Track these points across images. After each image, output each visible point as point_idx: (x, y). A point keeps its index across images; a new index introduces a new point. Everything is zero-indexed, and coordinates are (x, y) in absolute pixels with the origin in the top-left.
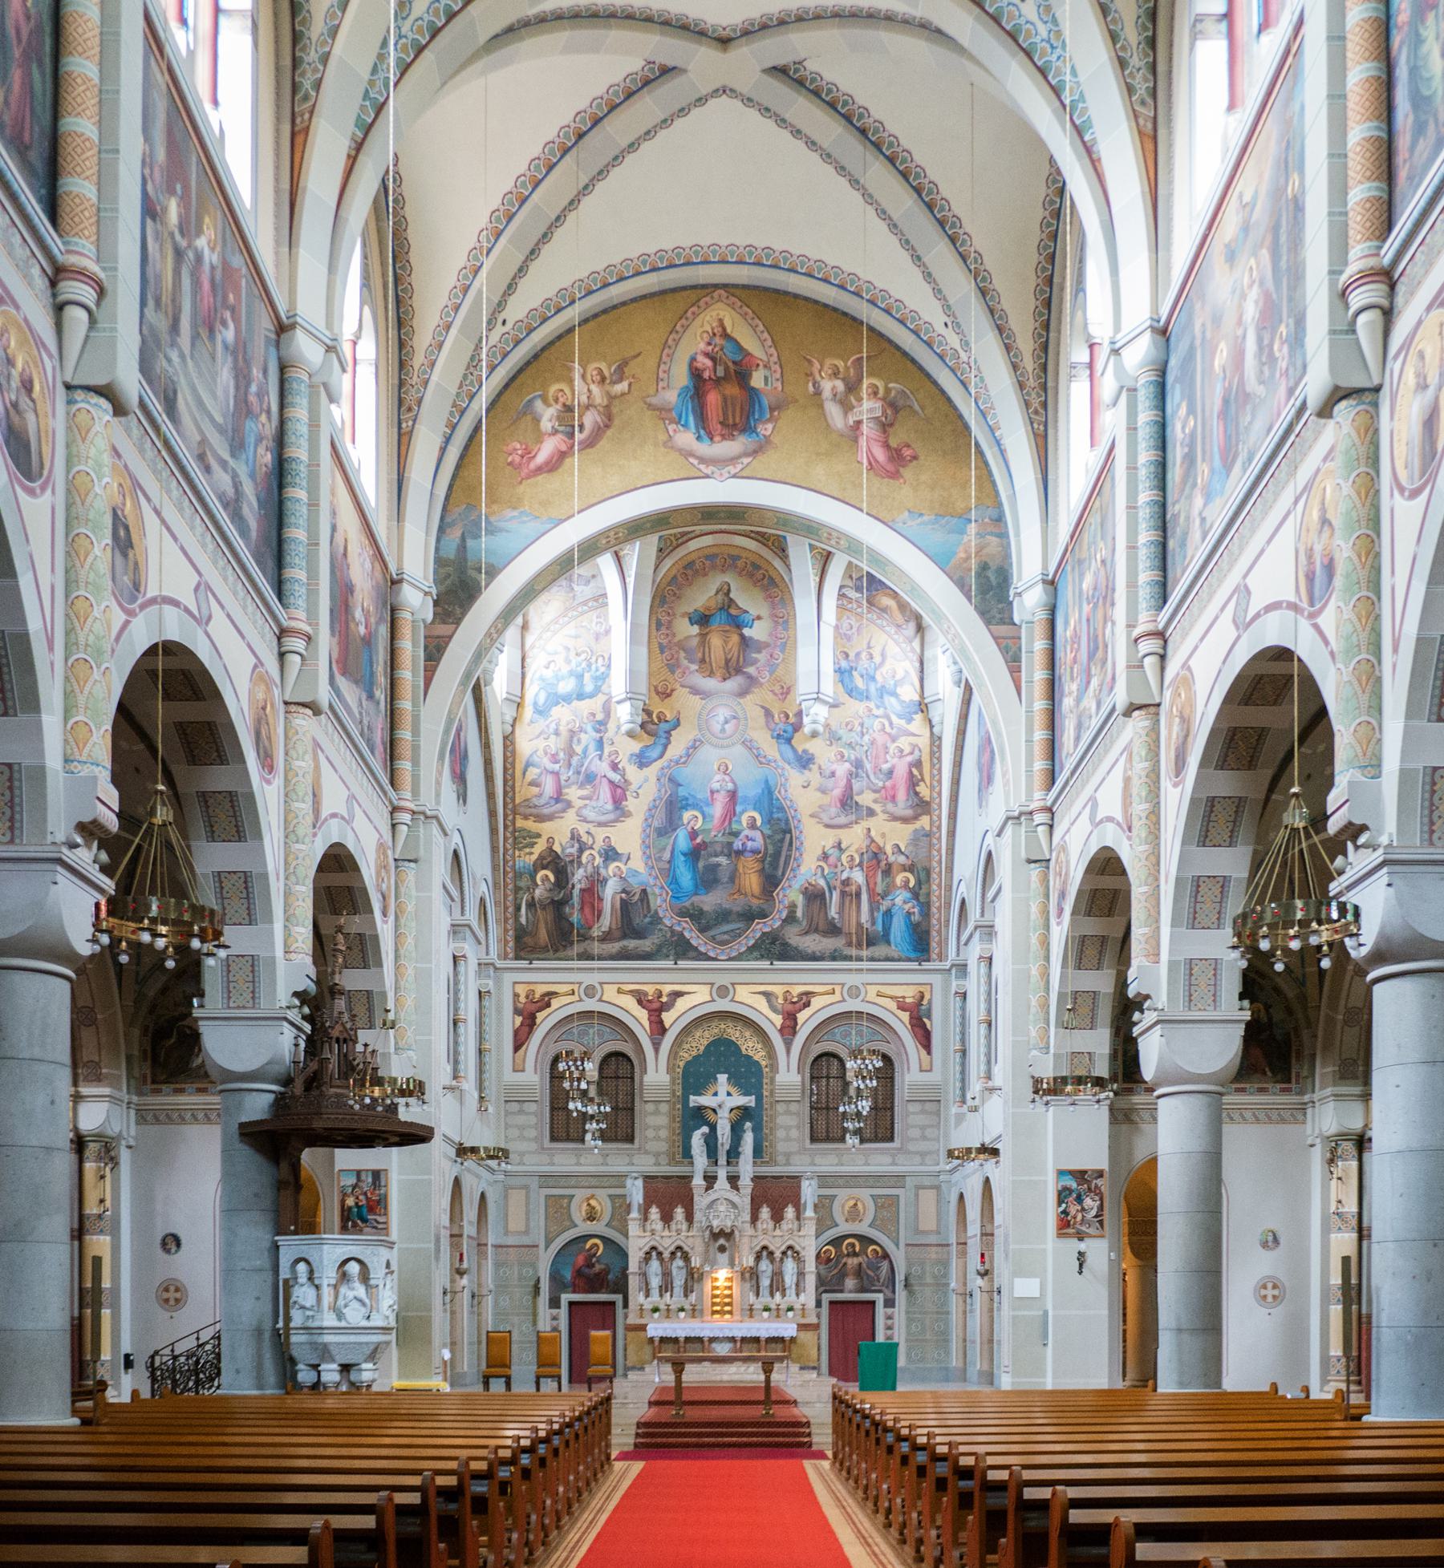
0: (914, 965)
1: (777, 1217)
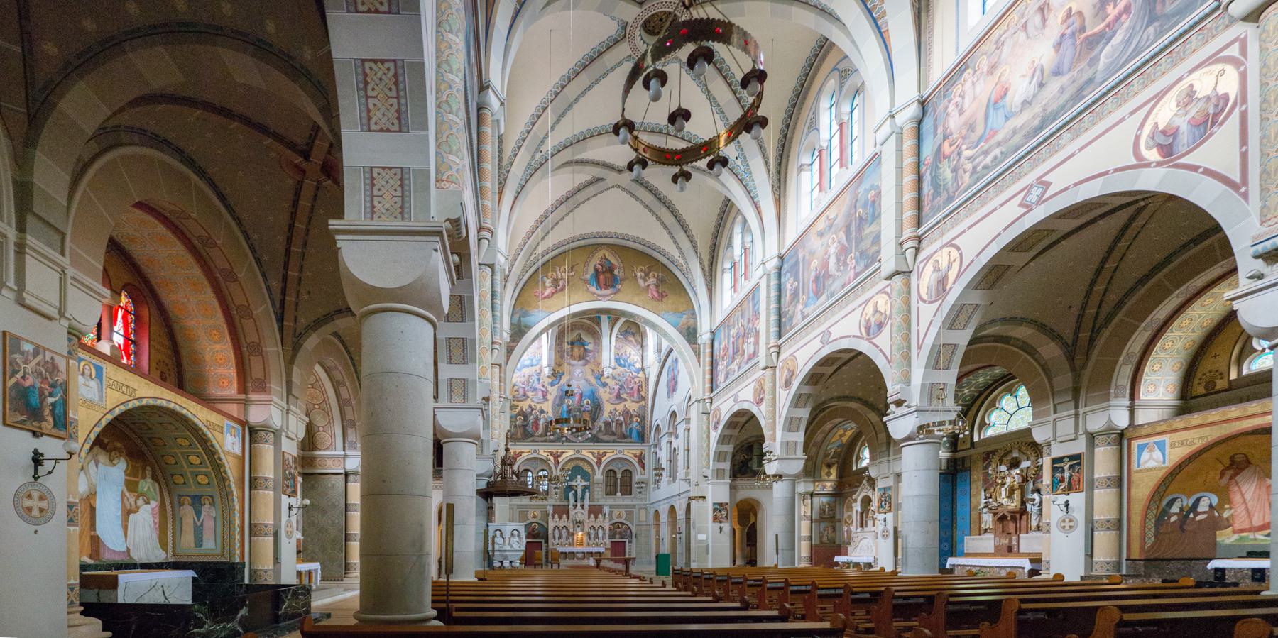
1: (596, 518)
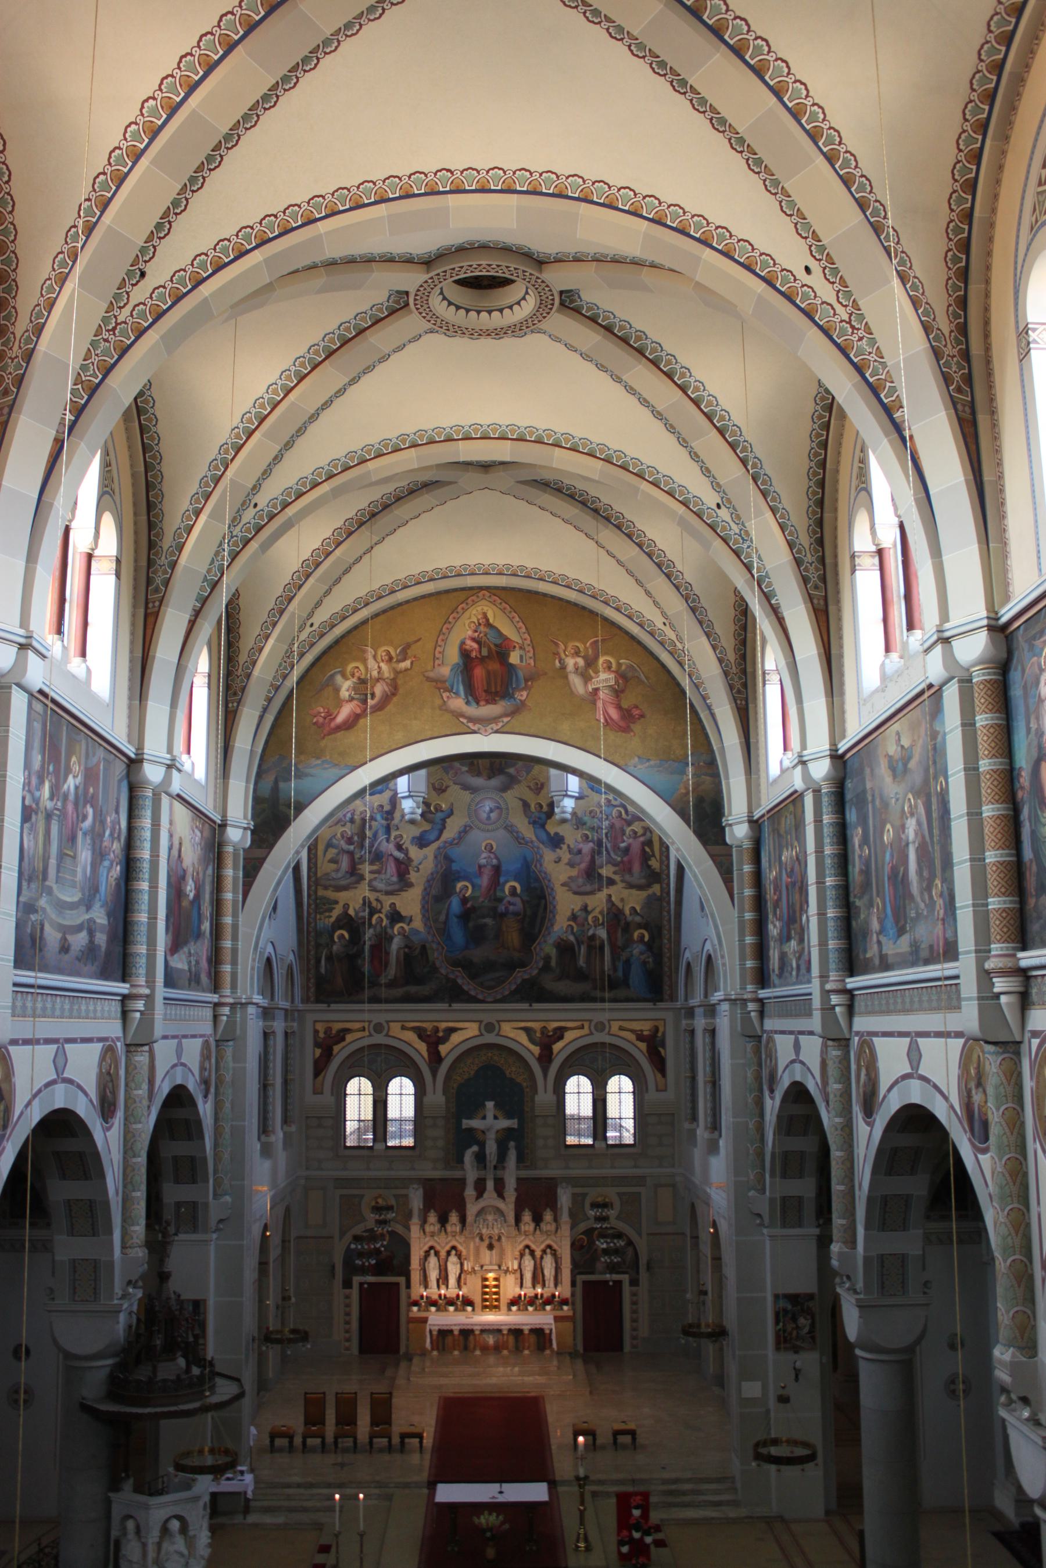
0: (649, 1005)
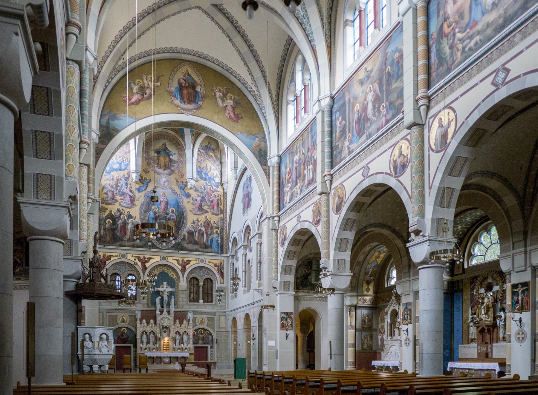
0: (219, 255)
1: (181, 323)
